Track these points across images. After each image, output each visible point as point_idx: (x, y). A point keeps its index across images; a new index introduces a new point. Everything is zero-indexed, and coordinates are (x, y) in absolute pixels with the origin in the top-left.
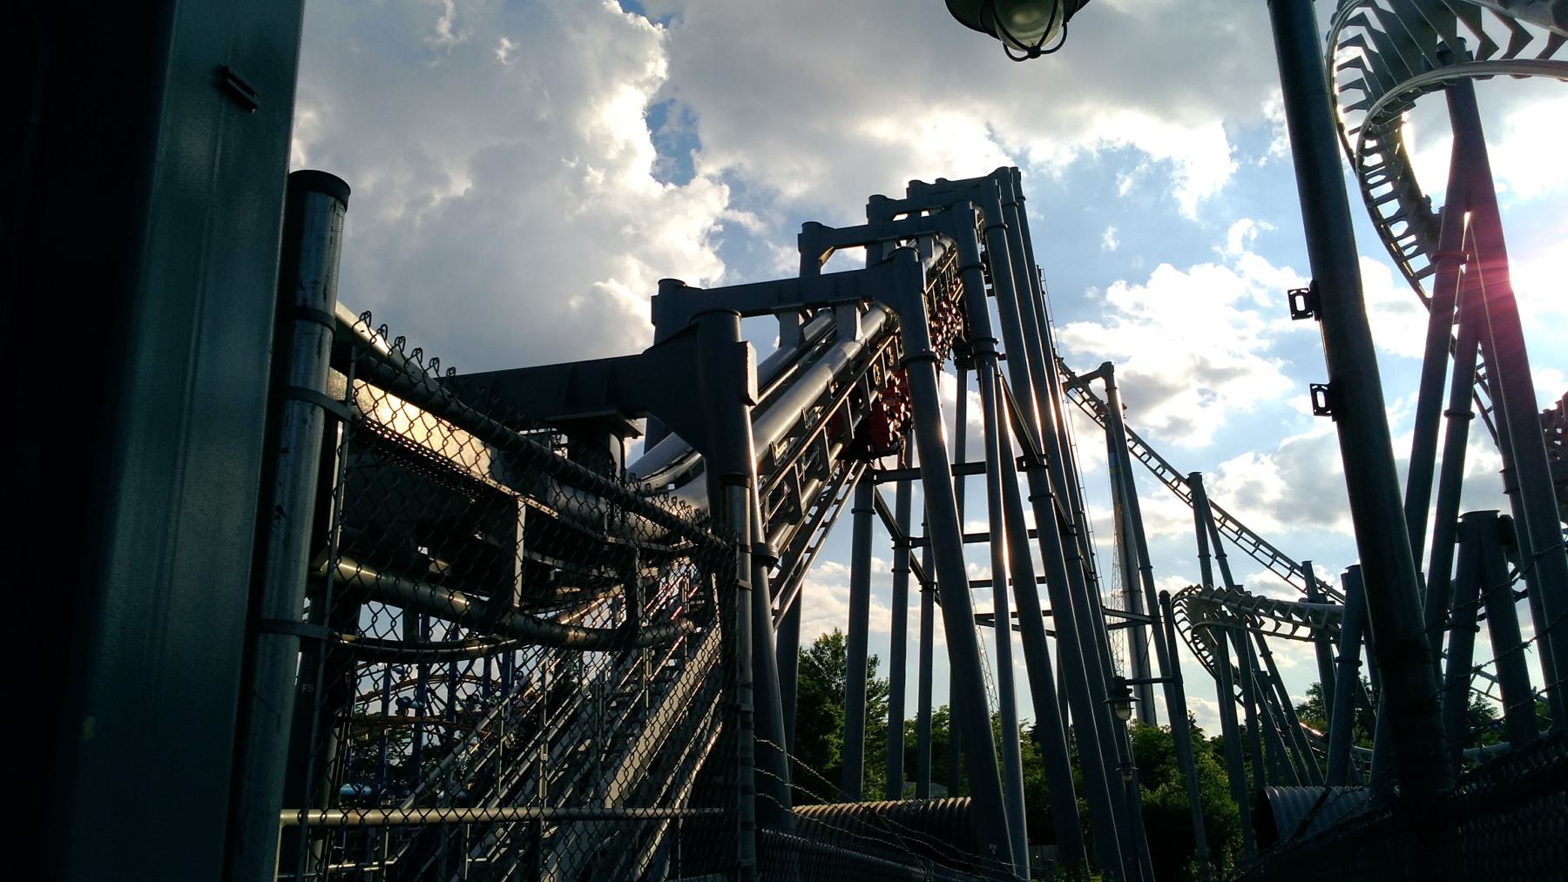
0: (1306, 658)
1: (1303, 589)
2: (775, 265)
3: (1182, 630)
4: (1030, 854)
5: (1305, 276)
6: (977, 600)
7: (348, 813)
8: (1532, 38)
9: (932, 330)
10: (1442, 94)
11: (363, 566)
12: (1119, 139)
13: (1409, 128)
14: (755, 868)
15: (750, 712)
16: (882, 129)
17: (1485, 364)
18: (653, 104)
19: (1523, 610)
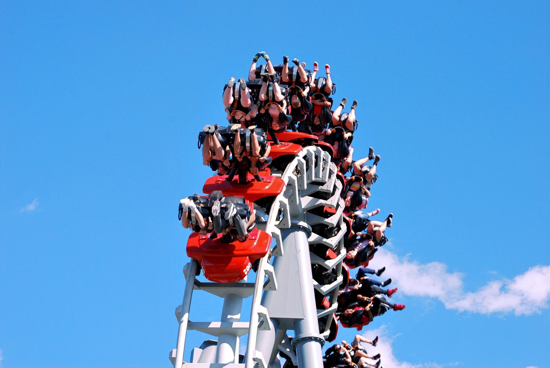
0: (238, 316)
1: (304, 131)
2: (246, 131)
3: (248, 330)
4: (295, 193)
5: (300, 146)
6: (260, 176)
7: (320, 124)
8: (239, 363)
9: (261, 143)
10: (249, 327)
11: (344, 138)
12: (285, 61)
13: (263, 169)
14: (317, 143)
15: (318, 143)
16: (246, 93)
17: (299, 124)
18: (372, 281)
19: (304, 101)
